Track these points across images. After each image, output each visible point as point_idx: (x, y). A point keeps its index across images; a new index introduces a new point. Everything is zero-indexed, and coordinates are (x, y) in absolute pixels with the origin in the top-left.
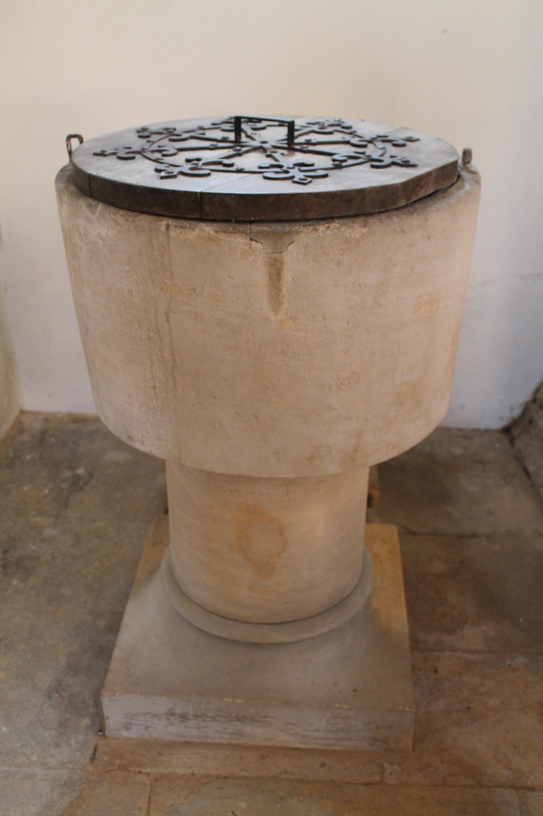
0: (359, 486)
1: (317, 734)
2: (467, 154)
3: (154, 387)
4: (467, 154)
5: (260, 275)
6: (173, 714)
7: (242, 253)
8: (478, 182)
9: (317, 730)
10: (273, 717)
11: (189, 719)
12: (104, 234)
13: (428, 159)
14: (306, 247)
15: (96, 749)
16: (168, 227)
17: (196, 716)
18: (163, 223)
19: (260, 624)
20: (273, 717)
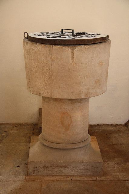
0: (90, 137)
1: (80, 171)
2: (108, 36)
3: (47, 80)
4: (108, 36)
5: (70, 55)
6: (45, 167)
7: (67, 50)
8: (110, 41)
9: (80, 170)
10: (69, 166)
11: (49, 168)
12: (39, 49)
13: (102, 35)
14: (78, 48)
15: (117, 144)
16: (53, 46)
17: (51, 167)
18: (51, 46)
19: (74, 143)
20: (69, 166)
